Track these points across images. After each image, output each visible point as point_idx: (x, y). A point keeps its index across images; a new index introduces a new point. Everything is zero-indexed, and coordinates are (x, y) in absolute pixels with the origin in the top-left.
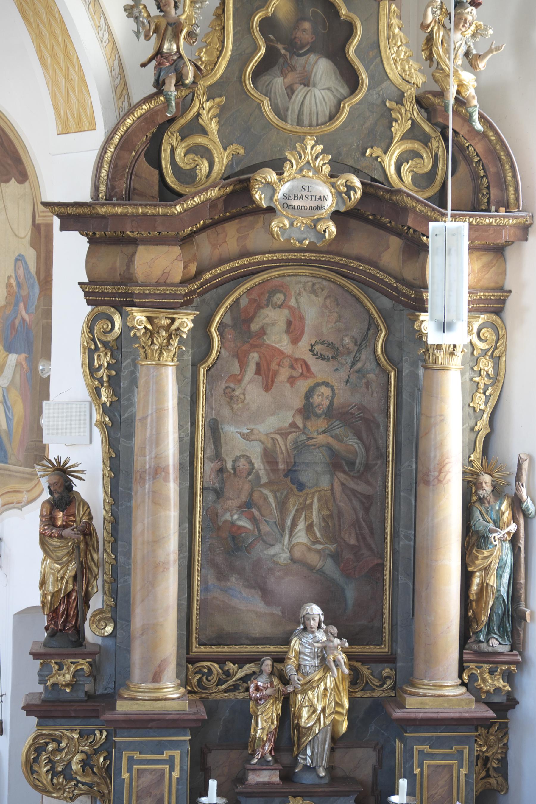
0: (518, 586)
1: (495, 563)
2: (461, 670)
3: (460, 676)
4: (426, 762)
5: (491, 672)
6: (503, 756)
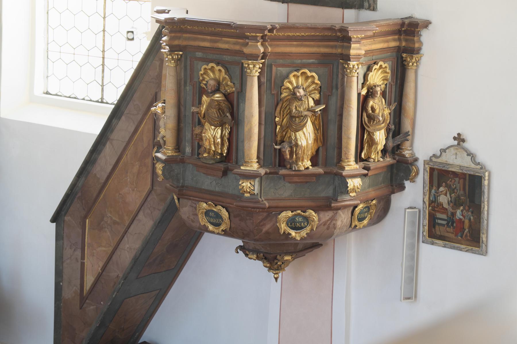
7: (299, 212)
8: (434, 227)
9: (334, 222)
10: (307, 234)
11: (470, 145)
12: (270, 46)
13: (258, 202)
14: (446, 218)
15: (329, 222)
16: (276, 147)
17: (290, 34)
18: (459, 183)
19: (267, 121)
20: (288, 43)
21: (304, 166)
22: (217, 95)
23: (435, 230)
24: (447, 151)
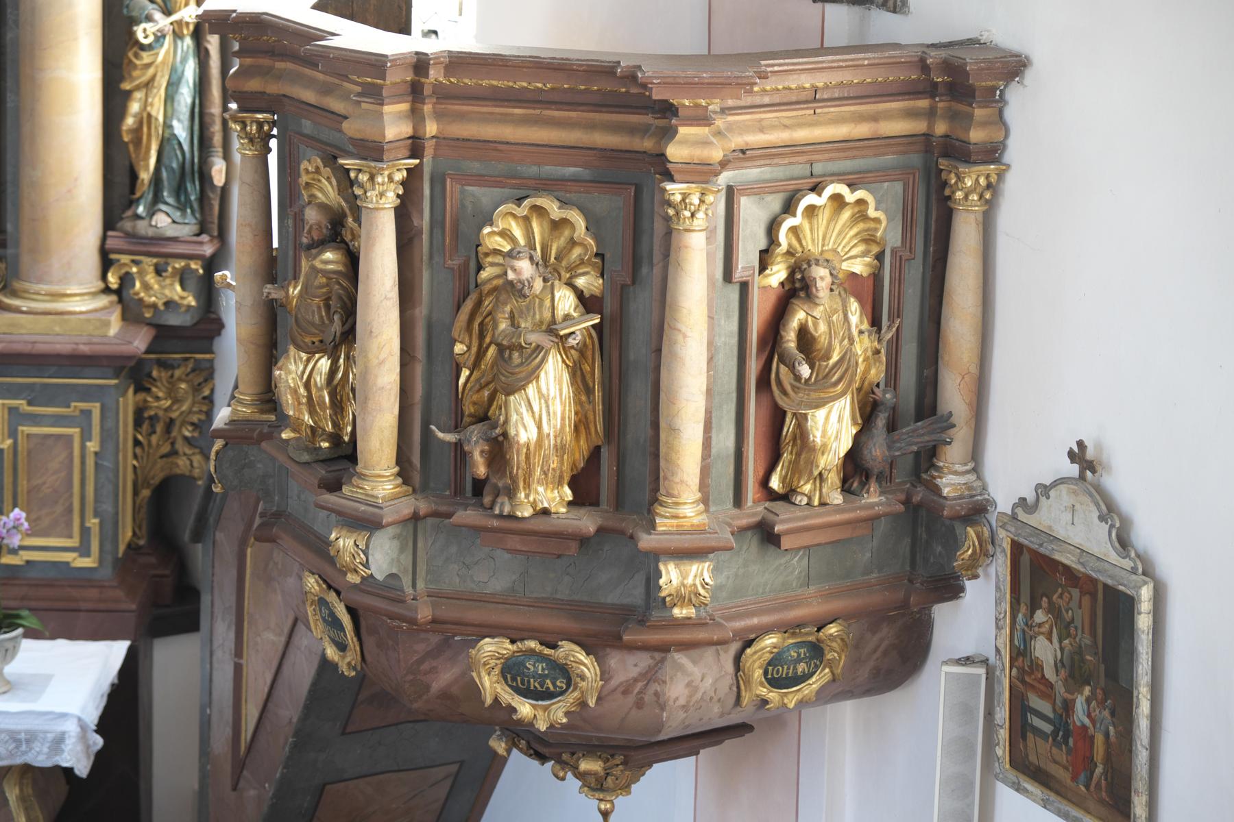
0: (207, 119)
1: (162, 76)
2: (106, 263)
3: (104, 277)
4: (25, 429)
5: (159, 271)
6: (203, 417)
7: (532, 644)
8: (1024, 737)
9: (655, 687)
10: (567, 714)
11: (1122, 483)
12: (439, 116)
13: (401, 601)
14: (1051, 715)
15: (640, 685)
17: (500, 84)
18: (1080, 607)
19: (421, 348)
20: (498, 110)
21: (534, 505)
22: (328, 255)
23: (1026, 746)
24: (1052, 493)
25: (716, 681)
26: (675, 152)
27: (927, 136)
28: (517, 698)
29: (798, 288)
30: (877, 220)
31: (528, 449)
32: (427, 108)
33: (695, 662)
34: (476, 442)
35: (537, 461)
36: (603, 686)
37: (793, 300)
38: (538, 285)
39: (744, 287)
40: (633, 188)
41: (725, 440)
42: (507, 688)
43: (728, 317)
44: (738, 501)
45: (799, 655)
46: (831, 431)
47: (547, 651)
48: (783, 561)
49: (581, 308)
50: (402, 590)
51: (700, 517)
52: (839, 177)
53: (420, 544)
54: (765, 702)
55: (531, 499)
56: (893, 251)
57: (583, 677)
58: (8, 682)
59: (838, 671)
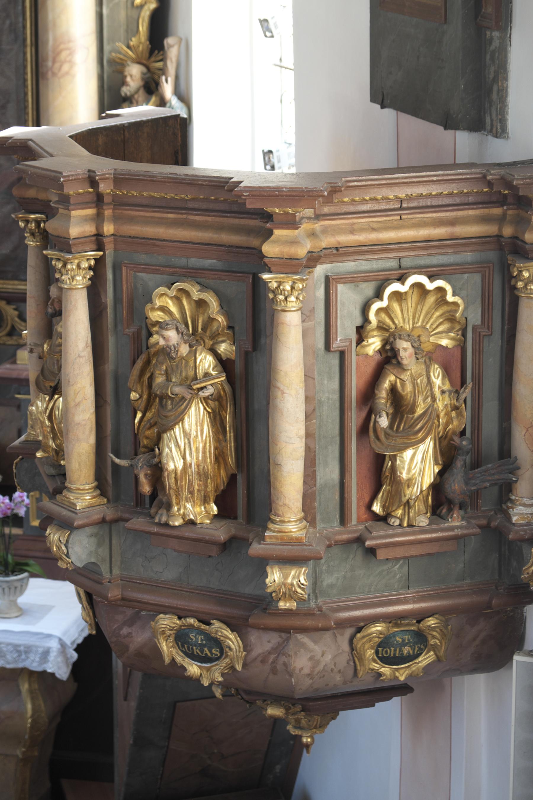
10: (223, 675)
12: (116, 219)
15: (272, 657)
16: (117, 461)
25: (335, 657)
26: (270, 249)
27: (499, 236)
28: (187, 660)
29: (389, 357)
30: (455, 304)
31: (176, 475)
32: (108, 212)
33: (315, 642)
34: (142, 467)
35: (185, 484)
36: (246, 656)
37: (387, 367)
38: (184, 350)
39: (342, 354)
40: (251, 276)
41: (329, 473)
42: (180, 652)
43: (330, 378)
44: (343, 520)
45: (403, 640)
46: (415, 471)
47: (203, 627)
48: (385, 567)
49: (220, 368)
50: (101, 575)
51: (301, 532)
52: (419, 269)
53: (114, 542)
54: (380, 675)
55: (182, 512)
56: (474, 328)
57: (230, 649)
58: (20, 609)
59: (441, 653)
